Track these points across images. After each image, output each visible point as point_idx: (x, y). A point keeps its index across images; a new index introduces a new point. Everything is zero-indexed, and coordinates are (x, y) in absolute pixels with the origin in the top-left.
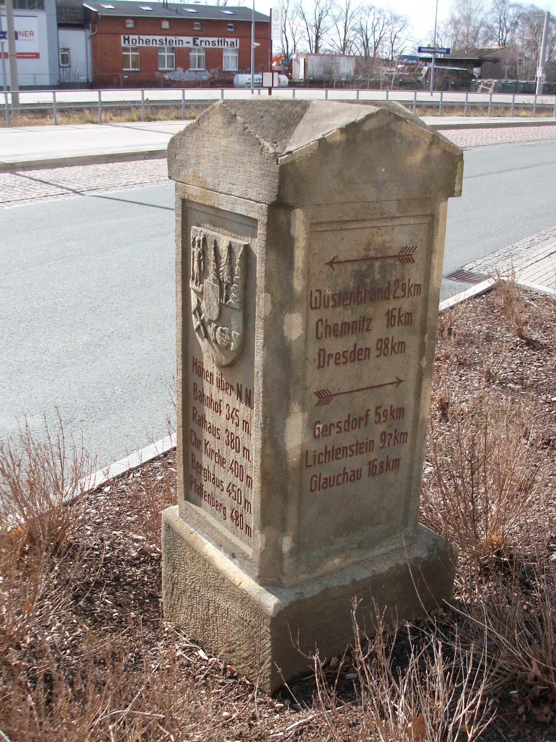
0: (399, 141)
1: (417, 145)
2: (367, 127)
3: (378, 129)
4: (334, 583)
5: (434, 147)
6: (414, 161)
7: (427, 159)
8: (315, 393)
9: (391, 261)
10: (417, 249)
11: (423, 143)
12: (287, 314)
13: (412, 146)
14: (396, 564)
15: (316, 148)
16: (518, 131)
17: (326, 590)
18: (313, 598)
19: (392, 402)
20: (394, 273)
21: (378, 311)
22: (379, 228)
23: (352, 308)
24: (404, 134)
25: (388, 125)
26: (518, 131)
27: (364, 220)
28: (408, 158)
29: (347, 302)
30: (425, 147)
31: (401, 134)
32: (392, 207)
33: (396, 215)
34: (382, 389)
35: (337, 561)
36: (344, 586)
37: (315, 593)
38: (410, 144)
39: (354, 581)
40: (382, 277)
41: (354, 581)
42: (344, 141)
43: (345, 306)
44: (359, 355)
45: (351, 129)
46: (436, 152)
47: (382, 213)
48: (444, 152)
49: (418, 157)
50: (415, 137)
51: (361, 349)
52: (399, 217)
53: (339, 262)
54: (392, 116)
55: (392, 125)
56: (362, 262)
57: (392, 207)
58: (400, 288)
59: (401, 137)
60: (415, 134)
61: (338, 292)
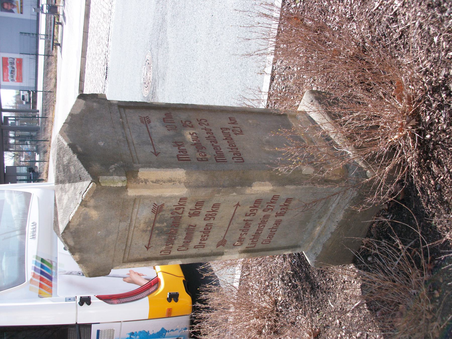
0: (82, 225)
1: (86, 214)
2: (72, 243)
3: (74, 238)
4: (324, 240)
5: (89, 204)
6: (96, 215)
7: (96, 207)
8: (217, 247)
9: (157, 219)
10: (156, 203)
11: (85, 211)
12: (151, 333)
13: (86, 218)
14: (345, 210)
15: (82, 265)
16: (90, 65)
17: (324, 246)
18: (321, 252)
19: (248, 207)
20: (166, 215)
21: (186, 220)
22: (135, 227)
23: (178, 235)
24: (78, 223)
25: (71, 233)
26: (90, 65)
27: (127, 239)
28: (94, 219)
29: (173, 238)
30: (88, 210)
31: (78, 225)
32: (123, 225)
33: (129, 222)
34: (236, 214)
35: (318, 229)
36: (330, 238)
37: (321, 250)
38: (84, 219)
39: (332, 233)
40: (166, 222)
41: (332, 233)
42: (79, 253)
43: (175, 239)
44: (233, 146)
45: (72, 250)
46: (92, 202)
47: (126, 230)
48: (93, 197)
49: (94, 214)
50: (80, 216)
51: (229, 145)
52: (131, 221)
53: (149, 244)
54: (66, 231)
55: (71, 230)
56: (153, 232)
57: (123, 225)
58: (177, 211)
59: (79, 225)
60: (78, 217)
61: (165, 243)
